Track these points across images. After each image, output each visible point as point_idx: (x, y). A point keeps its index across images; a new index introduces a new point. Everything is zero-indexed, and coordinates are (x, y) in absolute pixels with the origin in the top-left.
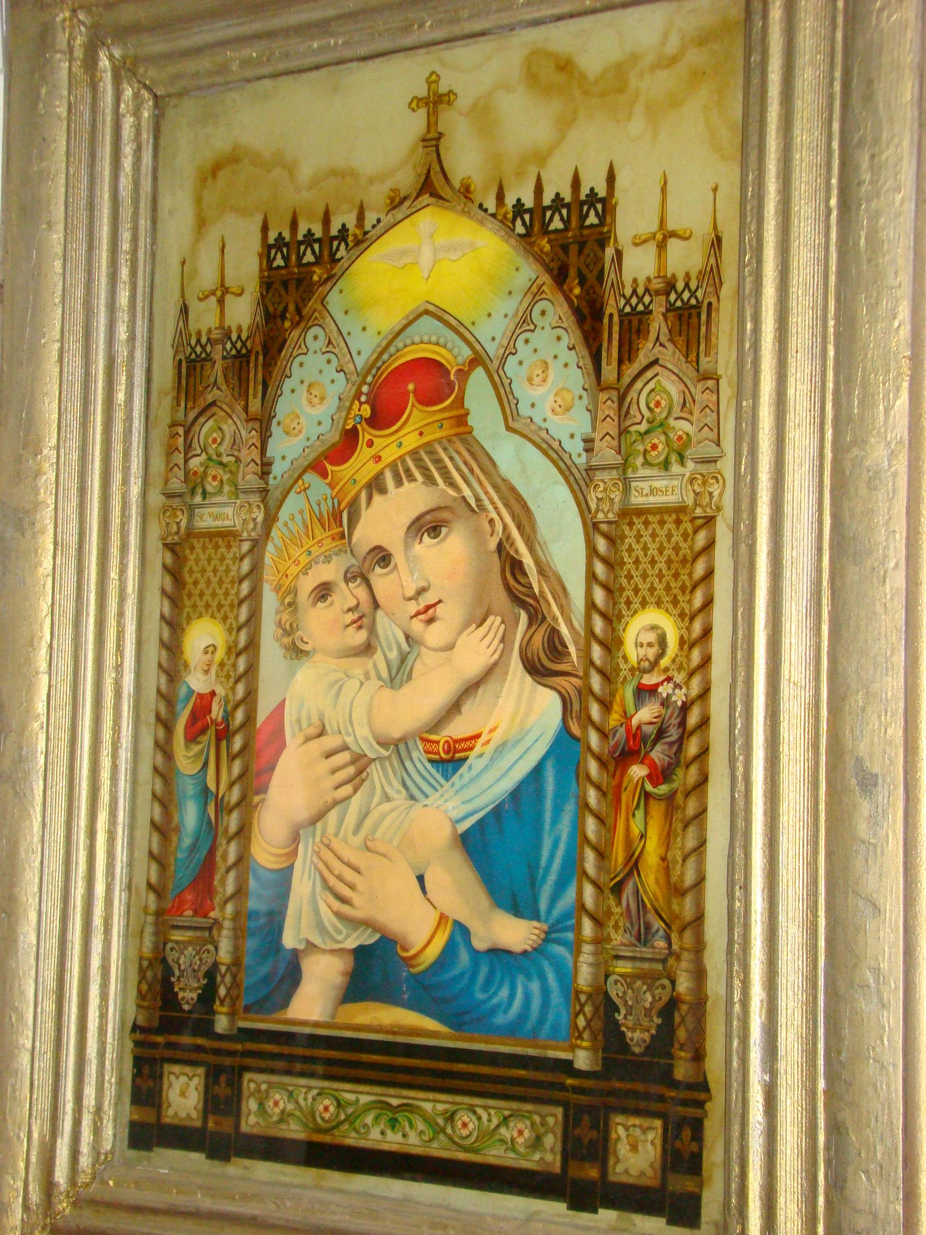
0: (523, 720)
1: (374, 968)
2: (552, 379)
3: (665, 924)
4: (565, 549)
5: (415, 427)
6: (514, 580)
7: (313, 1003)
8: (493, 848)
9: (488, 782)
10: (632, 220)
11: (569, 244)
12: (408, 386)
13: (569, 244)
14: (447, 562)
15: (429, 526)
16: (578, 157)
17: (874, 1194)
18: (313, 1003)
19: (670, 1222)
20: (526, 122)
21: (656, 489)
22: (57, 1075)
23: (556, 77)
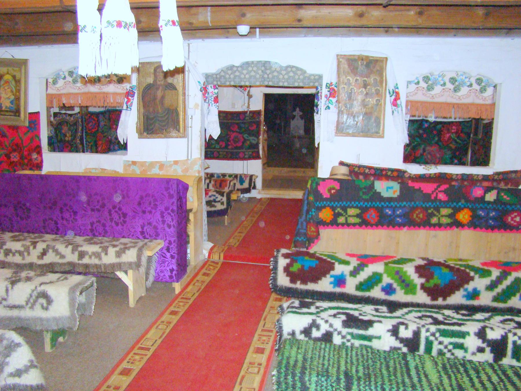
0: (13, 97)
1: (6, 107)
2: (13, 83)
3: (18, 106)
4: (14, 90)
5: (7, 84)
6: (12, 91)
7: (3, 109)
8: (12, 102)
9: (11, 99)
10: (17, 77)
11: (14, 77)
12: (7, 82)
13: (14, 77)
14: (9, 90)
15: (8, 88)
16: (14, 74)
17: (519, 4)
18: (3, 109)
19: (406, 146)
20: (12, 72)
21: (18, 88)
22: (191, 143)
23: (13, 70)
